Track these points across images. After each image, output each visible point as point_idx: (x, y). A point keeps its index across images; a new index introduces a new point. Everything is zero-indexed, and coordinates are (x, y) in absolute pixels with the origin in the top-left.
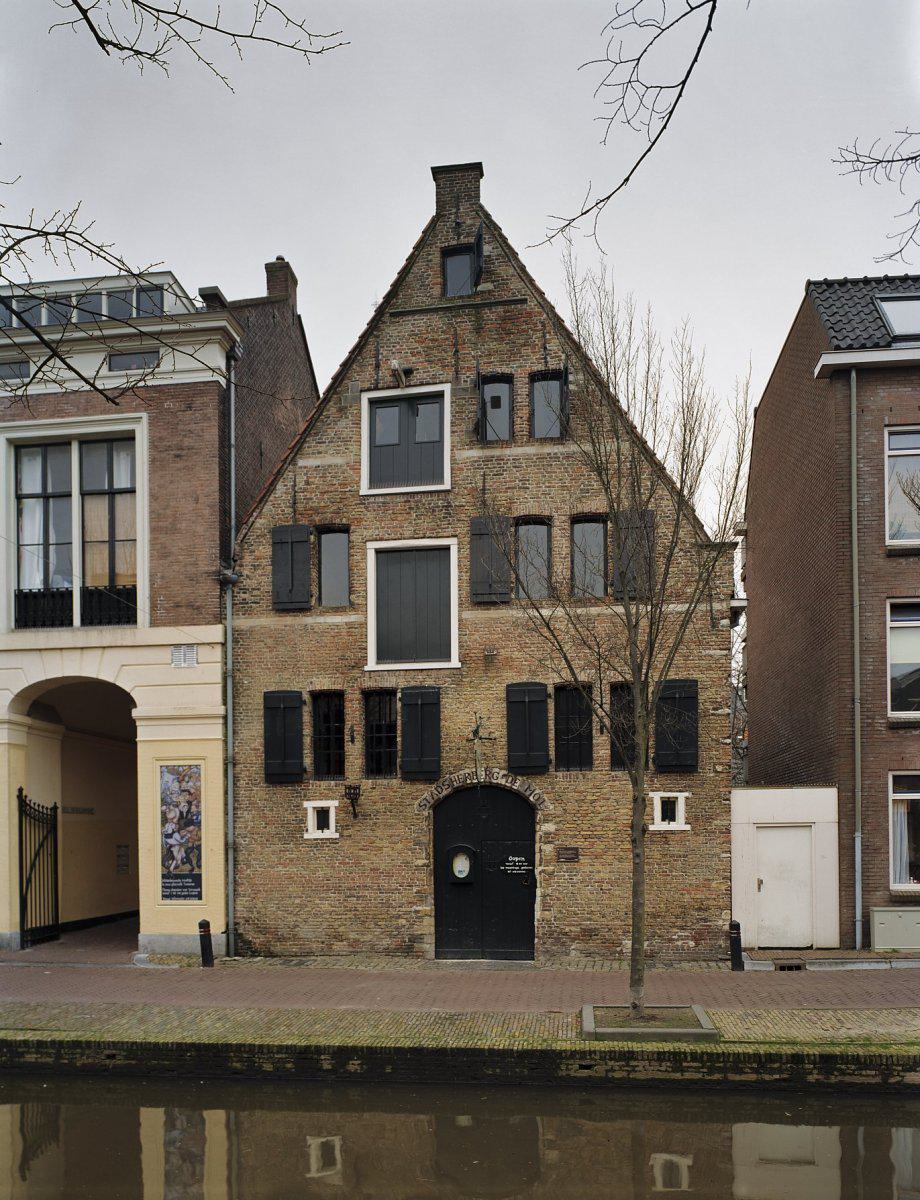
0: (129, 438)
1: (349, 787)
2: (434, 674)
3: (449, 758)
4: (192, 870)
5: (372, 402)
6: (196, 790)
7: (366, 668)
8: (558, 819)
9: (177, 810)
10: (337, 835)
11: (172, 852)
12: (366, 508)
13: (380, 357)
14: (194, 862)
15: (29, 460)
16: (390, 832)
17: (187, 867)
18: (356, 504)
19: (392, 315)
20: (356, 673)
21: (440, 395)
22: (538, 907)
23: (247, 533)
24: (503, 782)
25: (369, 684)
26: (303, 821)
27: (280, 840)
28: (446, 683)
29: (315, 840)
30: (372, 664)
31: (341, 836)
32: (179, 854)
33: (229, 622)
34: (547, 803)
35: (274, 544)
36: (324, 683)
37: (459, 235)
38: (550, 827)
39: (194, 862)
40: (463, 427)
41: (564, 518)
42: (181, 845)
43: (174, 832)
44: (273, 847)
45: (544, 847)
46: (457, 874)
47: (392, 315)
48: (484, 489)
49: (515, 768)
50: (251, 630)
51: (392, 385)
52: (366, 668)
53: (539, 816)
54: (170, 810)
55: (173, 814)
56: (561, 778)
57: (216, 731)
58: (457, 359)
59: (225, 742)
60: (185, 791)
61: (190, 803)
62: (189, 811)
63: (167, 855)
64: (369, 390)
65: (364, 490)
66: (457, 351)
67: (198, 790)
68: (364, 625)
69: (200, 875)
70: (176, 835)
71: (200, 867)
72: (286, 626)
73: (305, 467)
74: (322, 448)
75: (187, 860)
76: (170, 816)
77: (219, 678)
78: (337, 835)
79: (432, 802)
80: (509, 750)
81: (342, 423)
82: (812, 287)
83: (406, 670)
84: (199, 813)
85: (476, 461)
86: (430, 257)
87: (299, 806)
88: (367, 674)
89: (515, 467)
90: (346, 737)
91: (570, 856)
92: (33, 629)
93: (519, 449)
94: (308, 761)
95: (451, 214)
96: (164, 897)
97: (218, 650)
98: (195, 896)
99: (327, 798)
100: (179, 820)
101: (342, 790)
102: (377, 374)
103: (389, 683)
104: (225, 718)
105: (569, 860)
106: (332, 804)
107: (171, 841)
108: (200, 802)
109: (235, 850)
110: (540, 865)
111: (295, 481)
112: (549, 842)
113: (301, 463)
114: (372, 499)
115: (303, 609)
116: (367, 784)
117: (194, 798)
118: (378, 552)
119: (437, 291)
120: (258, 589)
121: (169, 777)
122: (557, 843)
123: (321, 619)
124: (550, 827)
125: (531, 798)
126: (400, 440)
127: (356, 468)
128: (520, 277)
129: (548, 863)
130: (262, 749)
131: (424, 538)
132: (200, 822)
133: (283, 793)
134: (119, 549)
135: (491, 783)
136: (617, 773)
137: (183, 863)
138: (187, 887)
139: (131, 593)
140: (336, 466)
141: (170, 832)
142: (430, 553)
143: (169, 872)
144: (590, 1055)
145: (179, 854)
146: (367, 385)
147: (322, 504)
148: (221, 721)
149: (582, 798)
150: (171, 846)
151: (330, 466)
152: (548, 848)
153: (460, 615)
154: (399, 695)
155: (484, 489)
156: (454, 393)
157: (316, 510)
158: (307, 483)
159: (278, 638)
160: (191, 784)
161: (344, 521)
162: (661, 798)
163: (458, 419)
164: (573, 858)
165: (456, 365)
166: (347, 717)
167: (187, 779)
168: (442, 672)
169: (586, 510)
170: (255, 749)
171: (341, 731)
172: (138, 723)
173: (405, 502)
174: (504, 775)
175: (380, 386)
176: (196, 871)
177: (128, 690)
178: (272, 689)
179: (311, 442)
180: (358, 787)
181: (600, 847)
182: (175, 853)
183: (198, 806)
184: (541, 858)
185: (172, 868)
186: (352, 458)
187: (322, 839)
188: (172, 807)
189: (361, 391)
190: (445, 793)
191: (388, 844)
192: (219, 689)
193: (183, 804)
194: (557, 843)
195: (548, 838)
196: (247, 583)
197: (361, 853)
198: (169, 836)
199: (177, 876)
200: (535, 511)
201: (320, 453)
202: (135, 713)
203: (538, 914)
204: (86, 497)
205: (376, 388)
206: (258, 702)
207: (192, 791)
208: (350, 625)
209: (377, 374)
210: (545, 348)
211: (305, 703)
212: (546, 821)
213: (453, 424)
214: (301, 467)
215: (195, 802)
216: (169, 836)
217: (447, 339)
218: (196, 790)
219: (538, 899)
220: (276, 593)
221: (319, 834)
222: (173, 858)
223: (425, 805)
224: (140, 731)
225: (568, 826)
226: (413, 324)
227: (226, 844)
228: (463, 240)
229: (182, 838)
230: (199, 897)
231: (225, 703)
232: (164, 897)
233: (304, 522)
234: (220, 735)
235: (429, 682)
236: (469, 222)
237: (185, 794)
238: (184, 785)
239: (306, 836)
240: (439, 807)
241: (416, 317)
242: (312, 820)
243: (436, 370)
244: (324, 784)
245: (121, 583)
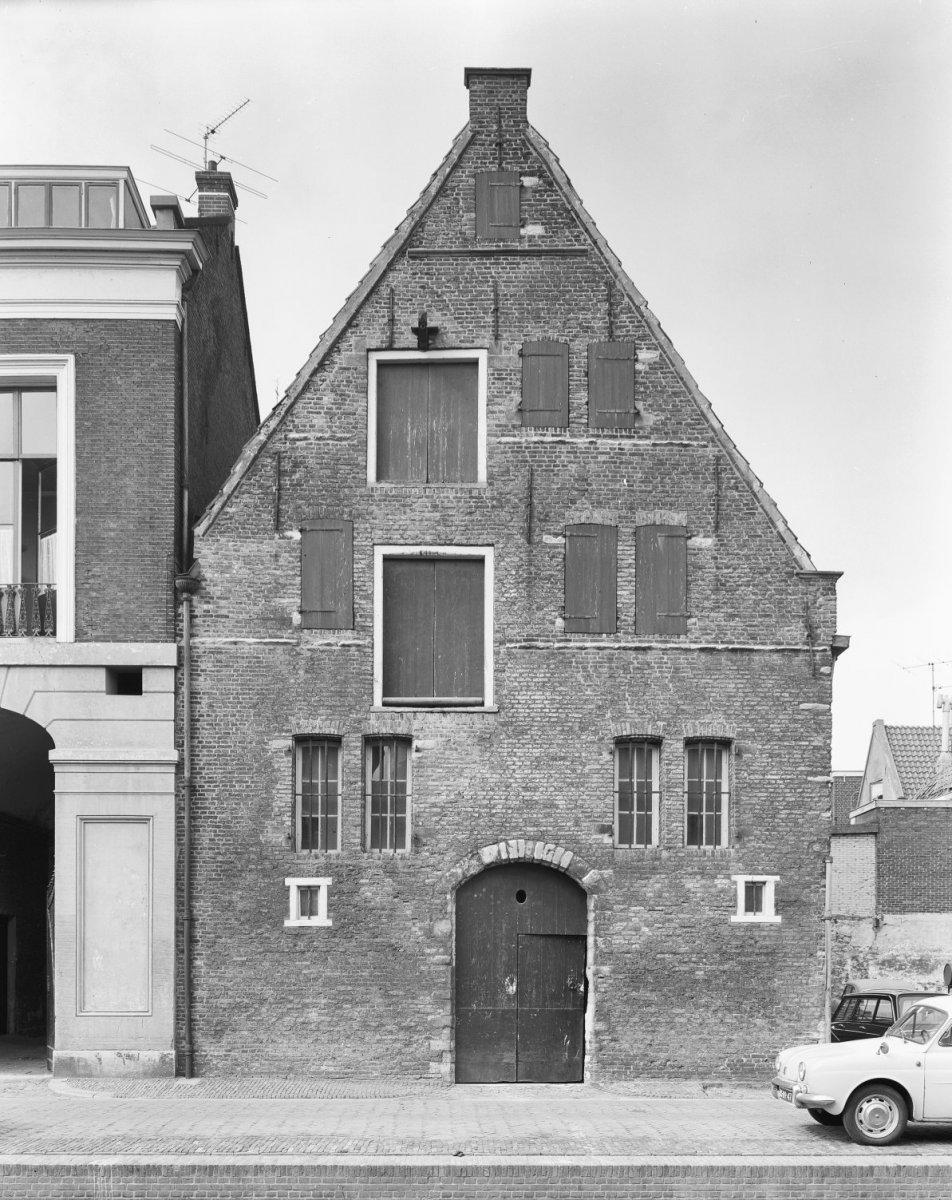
21: (474, 363)
57: (167, 781)
65: (488, 553)
68: (366, 652)
118: (387, 559)
148: (173, 769)
205: (390, 348)
231: (178, 745)
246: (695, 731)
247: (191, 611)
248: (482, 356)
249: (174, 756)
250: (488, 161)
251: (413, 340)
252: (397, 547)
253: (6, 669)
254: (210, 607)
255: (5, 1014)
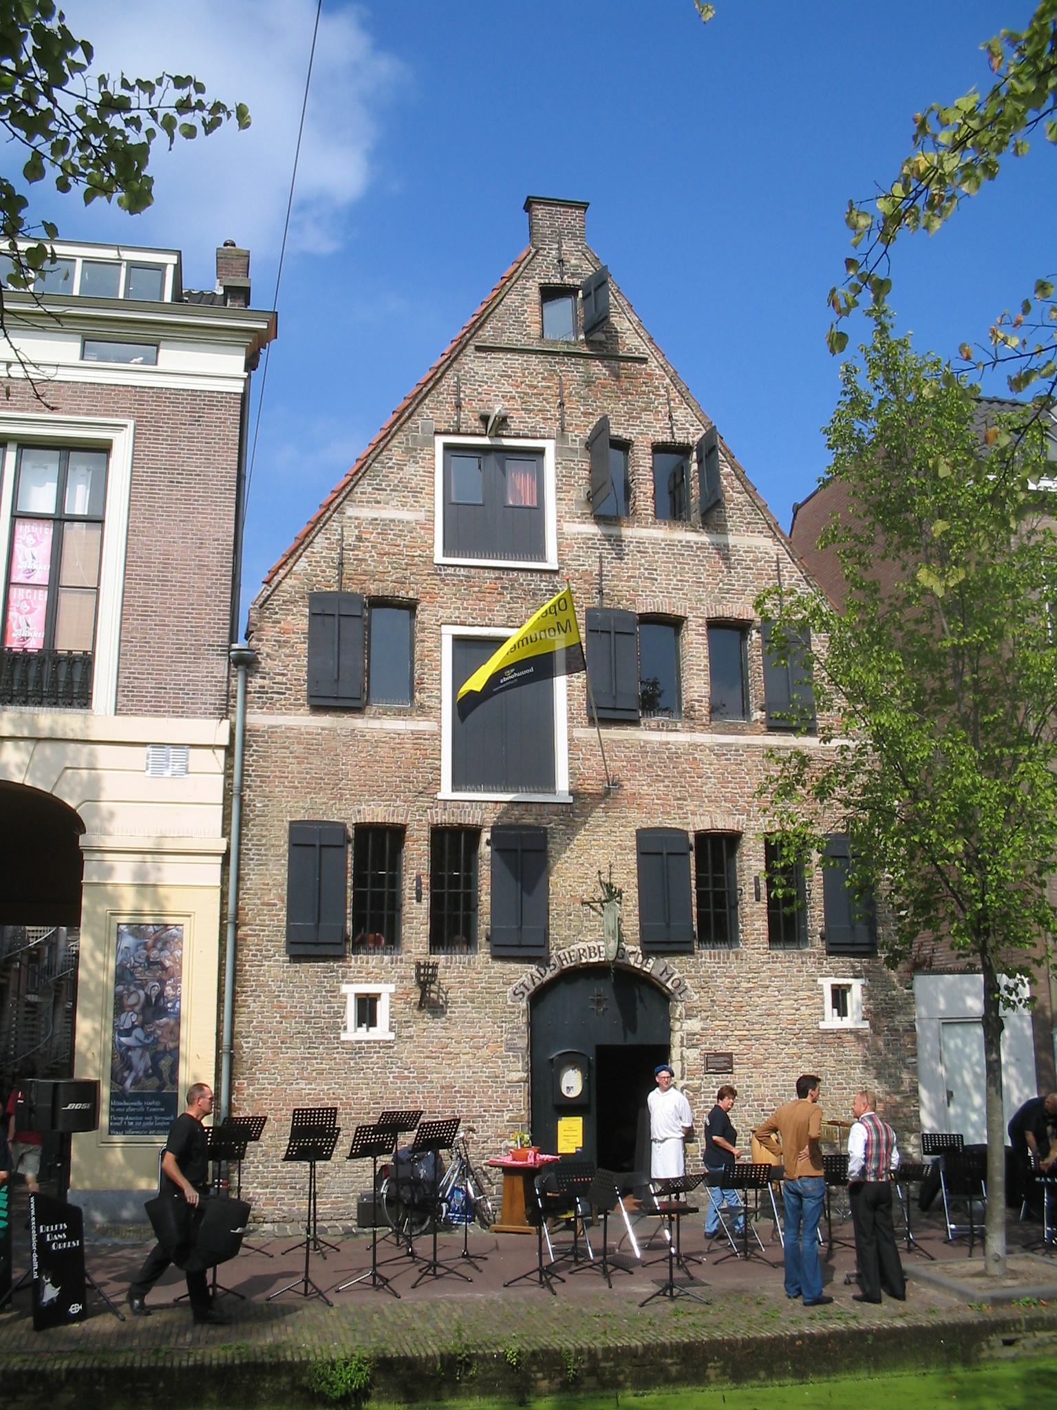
0: (103, 449)
2: (534, 809)
3: (556, 932)
4: (162, 1086)
7: (440, 796)
8: (704, 1014)
9: (141, 993)
12: (443, 580)
13: (462, 395)
15: (34, 467)
16: (471, 1032)
17: (155, 1081)
18: (429, 575)
19: (478, 349)
20: (424, 801)
21: (540, 452)
23: (269, 596)
25: (443, 818)
26: (339, 1014)
27: (302, 1043)
29: (358, 1042)
30: (446, 791)
31: (399, 1036)
32: (141, 1062)
33: (237, 717)
34: (691, 992)
35: (313, 615)
36: (376, 812)
37: (562, 274)
38: (694, 1025)
40: (574, 494)
41: (701, 621)
42: (145, 1047)
43: (134, 1027)
44: (291, 1054)
45: (687, 1052)
46: (564, 1091)
47: (478, 349)
48: (600, 575)
49: (651, 948)
50: (272, 730)
52: (440, 796)
53: (680, 1009)
54: (130, 994)
56: (707, 958)
57: (211, 871)
58: (563, 414)
64: (446, 433)
65: (439, 558)
66: (562, 404)
68: (437, 736)
70: (138, 1032)
72: (323, 729)
73: (357, 518)
74: (381, 496)
75: (155, 1070)
77: (219, 798)
78: (391, 1036)
79: (532, 988)
80: (290, 917)
81: (410, 469)
82: (243, 261)
83: (497, 802)
85: (589, 539)
86: (526, 291)
87: (334, 992)
88: (441, 805)
89: (639, 552)
93: (644, 530)
95: (551, 249)
97: (221, 754)
99: (377, 980)
102: (458, 415)
103: (471, 818)
104: (226, 857)
110: (682, 1078)
111: (342, 535)
112: (694, 1046)
113: (350, 511)
114: (451, 570)
115: (355, 708)
118: (458, 640)
119: (535, 329)
120: (283, 675)
122: (703, 1046)
123: (375, 724)
124: (694, 1025)
125: (669, 985)
126: (484, 501)
127: (428, 526)
128: (637, 333)
129: (692, 1074)
134: (67, 601)
136: (777, 952)
137: (148, 1076)
139: (86, 662)
140: (401, 521)
141: (128, 1025)
143: (123, 1091)
144: (1014, 1326)
147: (381, 569)
148: (219, 860)
149: (735, 985)
151: (392, 521)
152: (692, 1054)
153: (570, 733)
154: (486, 836)
155: (600, 575)
156: (559, 452)
157: (372, 576)
158: (359, 539)
159: (312, 745)
161: (411, 595)
162: (832, 985)
163: (565, 484)
164: (726, 1068)
165: (562, 419)
168: (546, 807)
169: (727, 614)
170: (269, 905)
173: (496, 578)
179: (365, 486)
181: (758, 1052)
183: (175, 988)
184: (683, 1068)
185: (128, 1083)
186: (421, 516)
187: (368, 1042)
188: (132, 988)
191: (468, 1050)
192: (219, 810)
194: (703, 1046)
195: (692, 1041)
196: (265, 664)
197: (429, 1063)
200: (665, 609)
201: (379, 502)
204: (18, 521)
205: (457, 433)
208: (417, 735)
209: (458, 415)
210: (670, 417)
212: (689, 1017)
213: (558, 489)
214: (350, 518)
217: (549, 387)
220: (313, 679)
221: (363, 1034)
222: (130, 1067)
223: (523, 993)
225: (717, 1023)
226: (504, 364)
228: (568, 280)
229: (147, 1036)
231: (226, 833)
233: (352, 588)
235: (529, 820)
236: (573, 262)
239: (344, 1037)
240: (538, 997)
241: (509, 356)
242: (383, 1010)
243: (534, 420)
245: (64, 644)
246: (424, 864)
247: (246, 687)
248: (549, 446)
249: (221, 845)
250: (602, 381)
251: (476, 425)
252: (477, 628)
253: (34, 742)
254: (266, 682)
255: (697, 866)
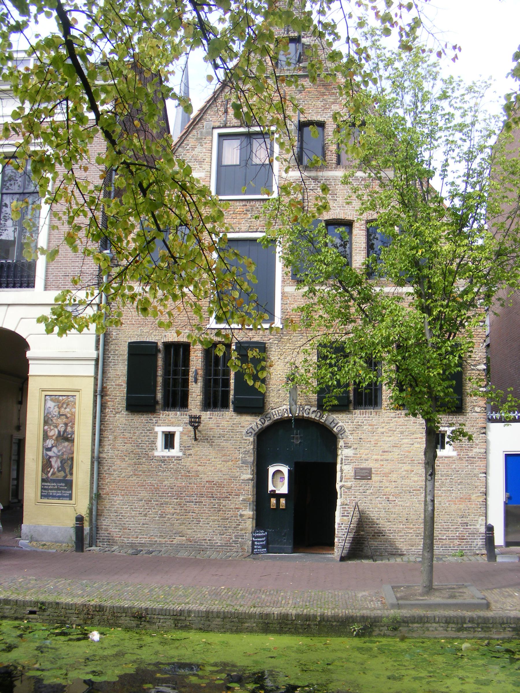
1: (191, 417)
4: (66, 476)
5: (220, 136)
6: (72, 415)
9: (56, 430)
10: (180, 454)
11: (50, 462)
14: (68, 470)
17: (62, 474)
22: (338, 514)
24: (313, 416)
26: (154, 442)
28: (269, 339)
29: (163, 457)
32: (56, 464)
36: (171, 337)
39: (68, 470)
42: (58, 457)
43: (53, 447)
51: (236, 125)
53: (341, 443)
55: (53, 432)
57: (89, 369)
59: (96, 379)
60: (63, 415)
61: (66, 425)
62: (65, 431)
63: (47, 464)
64: (219, 127)
67: (73, 414)
69: (72, 481)
70: (55, 449)
71: (71, 474)
75: (62, 468)
76: (51, 434)
78: (180, 454)
79: (257, 430)
84: (73, 433)
87: (151, 430)
90: (190, 378)
91: (365, 475)
92: (19, 289)
94: (159, 396)
96: (42, 496)
98: (67, 497)
100: (57, 438)
101: (187, 419)
104: (97, 360)
105: (363, 478)
106: (178, 430)
107: (50, 453)
108: (74, 424)
109: (99, 463)
116: (206, 416)
117: (70, 421)
121: (51, 404)
125: (335, 429)
130: (125, 385)
131: (256, 232)
132: (73, 440)
133: (140, 420)
135: (303, 416)
137: (59, 471)
138: (63, 489)
141: (50, 446)
142: (240, 242)
143: (48, 477)
145: (56, 464)
146: (217, 124)
148: (93, 363)
150: (50, 457)
153: (283, 289)
154: (233, 347)
160: (68, 410)
164: (367, 476)
166: (191, 363)
167: (65, 406)
170: (119, 385)
171: (186, 373)
172: (30, 362)
173: (243, 206)
174: (314, 411)
175: (228, 125)
176: (69, 478)
177: (24, 337)
178: (134, 340)
180: (199, 417)
182: (53, 463)
183: (72, 427)
185: (50, 474)
187: (168, 457)
188: (52, 427)
189: (213, 128)
190: (267, 423)
193: (61, 425)
198: (49, 449)
199: (54, 481)
200: (341, 216)
202: (29, 354)
203: (338, 519)
205: (225, 127)
206: (124, 351)
207: (69, 415)
211: (159, 351)
215: (70, 424)
216: (49, 449)
218: (72, 415)
219: (338, 508)
221: (167, 453)
222: (51, 467)
224: (31, 367)
227: (93, 457)
229: (59, 451)
230: (70, 497)
231: (97, 348)
232: (42, 496)
234: (92, 373)
237: (63, 417)
238: (63, 411)
242: (160, 441)
244: (172, 414)
